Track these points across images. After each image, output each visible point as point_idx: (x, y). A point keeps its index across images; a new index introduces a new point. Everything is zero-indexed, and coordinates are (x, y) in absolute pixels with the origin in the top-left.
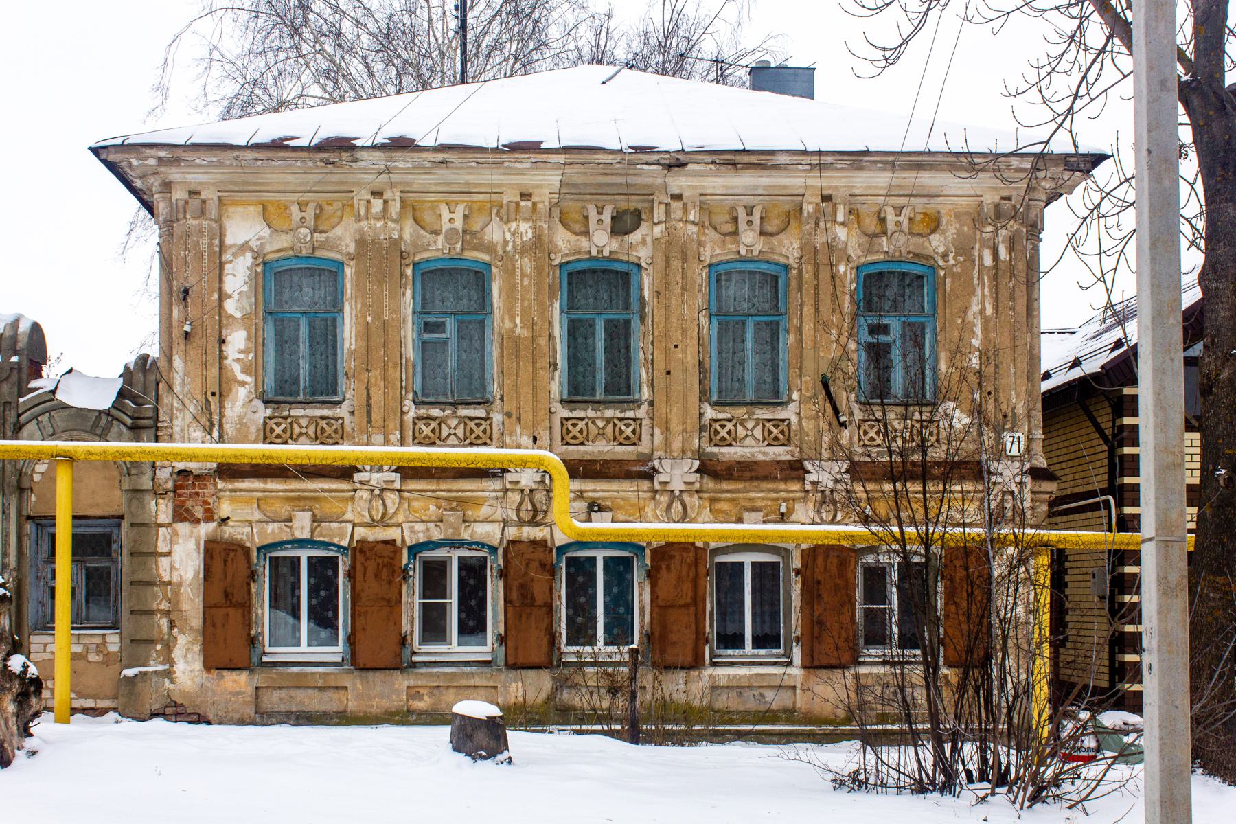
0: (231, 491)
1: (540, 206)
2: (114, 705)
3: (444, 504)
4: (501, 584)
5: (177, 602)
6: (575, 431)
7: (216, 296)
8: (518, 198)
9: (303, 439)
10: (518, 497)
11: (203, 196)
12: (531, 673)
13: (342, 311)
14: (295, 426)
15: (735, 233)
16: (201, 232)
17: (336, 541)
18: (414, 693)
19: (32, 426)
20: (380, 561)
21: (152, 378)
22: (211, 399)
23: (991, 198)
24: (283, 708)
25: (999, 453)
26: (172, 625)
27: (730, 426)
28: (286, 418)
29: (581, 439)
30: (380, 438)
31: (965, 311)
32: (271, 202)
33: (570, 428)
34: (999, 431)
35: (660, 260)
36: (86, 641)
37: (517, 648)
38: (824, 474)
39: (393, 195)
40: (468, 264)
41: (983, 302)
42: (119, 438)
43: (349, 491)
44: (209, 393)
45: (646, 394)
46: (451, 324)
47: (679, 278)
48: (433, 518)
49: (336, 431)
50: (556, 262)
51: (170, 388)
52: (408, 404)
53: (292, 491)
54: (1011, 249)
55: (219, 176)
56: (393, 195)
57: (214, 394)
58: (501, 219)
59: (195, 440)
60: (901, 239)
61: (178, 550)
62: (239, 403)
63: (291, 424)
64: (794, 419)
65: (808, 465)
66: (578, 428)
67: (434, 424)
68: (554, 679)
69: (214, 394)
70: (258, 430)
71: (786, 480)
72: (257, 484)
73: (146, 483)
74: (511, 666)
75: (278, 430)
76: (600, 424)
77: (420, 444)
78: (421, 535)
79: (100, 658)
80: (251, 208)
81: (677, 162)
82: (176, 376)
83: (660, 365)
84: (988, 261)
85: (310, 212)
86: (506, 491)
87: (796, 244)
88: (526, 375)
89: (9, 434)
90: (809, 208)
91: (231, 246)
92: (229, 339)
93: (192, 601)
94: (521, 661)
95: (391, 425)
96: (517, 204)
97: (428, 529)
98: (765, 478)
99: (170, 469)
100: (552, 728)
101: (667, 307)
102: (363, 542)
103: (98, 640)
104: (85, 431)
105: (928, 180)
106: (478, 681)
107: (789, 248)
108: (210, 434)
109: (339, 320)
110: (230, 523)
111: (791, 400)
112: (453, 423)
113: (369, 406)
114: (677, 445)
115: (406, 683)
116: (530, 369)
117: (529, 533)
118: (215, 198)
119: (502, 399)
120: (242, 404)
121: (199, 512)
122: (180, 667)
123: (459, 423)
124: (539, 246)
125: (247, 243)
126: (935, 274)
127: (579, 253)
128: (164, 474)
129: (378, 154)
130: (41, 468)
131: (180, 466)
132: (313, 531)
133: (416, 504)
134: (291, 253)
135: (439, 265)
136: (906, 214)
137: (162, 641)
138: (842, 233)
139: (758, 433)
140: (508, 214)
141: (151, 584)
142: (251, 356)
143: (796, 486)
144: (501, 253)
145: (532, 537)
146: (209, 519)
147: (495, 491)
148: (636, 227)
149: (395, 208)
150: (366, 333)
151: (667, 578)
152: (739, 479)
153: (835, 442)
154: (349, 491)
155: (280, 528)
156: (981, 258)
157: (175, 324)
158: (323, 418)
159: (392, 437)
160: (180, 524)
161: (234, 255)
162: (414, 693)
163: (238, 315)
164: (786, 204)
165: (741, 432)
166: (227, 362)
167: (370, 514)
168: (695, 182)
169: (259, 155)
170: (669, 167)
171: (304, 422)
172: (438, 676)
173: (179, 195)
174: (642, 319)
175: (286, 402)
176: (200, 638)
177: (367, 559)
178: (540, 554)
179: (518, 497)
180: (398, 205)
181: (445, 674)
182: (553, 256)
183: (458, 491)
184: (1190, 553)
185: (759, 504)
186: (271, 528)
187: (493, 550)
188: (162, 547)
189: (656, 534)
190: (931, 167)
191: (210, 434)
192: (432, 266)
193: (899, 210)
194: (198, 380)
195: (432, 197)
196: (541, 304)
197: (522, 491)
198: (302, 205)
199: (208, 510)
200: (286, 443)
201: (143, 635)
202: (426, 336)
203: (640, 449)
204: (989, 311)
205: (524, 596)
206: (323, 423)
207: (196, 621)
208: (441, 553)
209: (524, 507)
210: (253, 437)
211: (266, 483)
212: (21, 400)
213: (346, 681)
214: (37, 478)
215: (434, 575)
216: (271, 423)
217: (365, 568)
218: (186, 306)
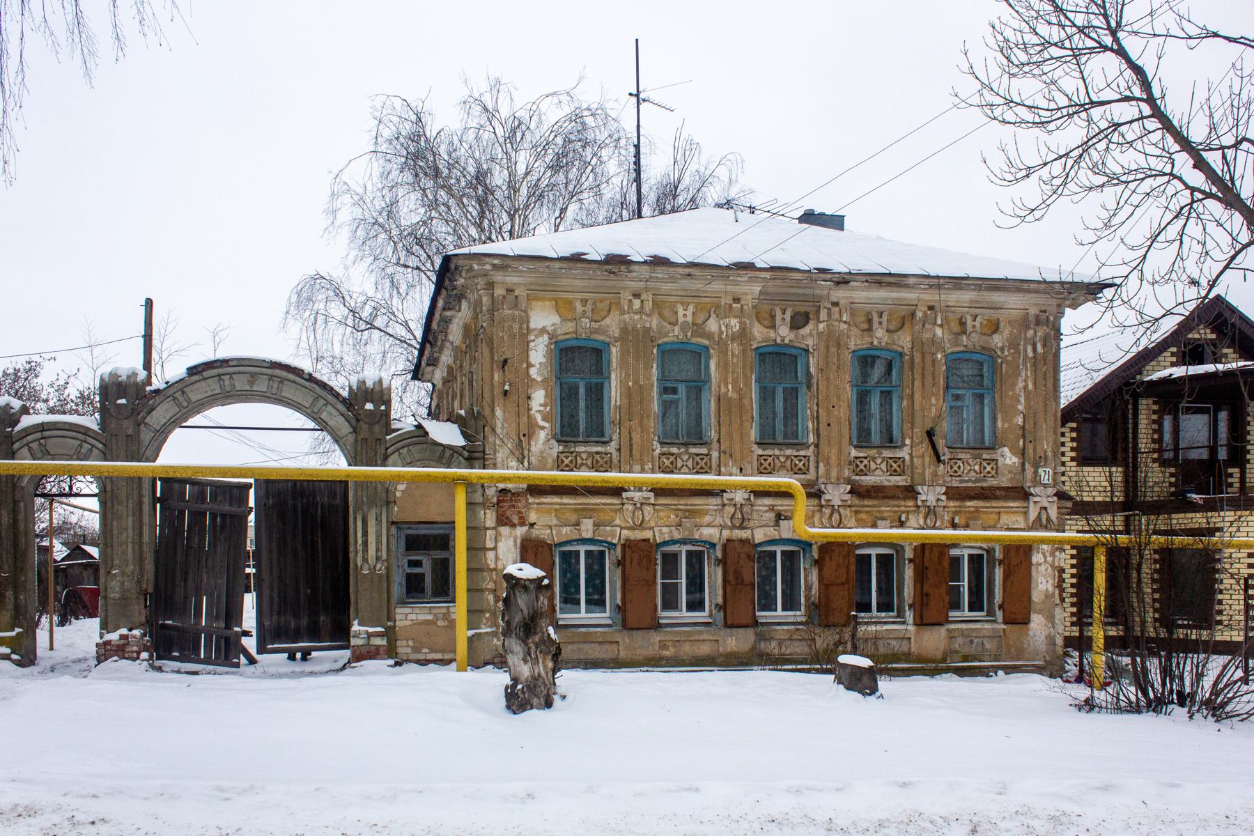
3: (680, 513)
4: (719, 571)
6: (766, 464)
9: (583, 468)
10: (732, 510)
12: (741, 631)
15: (870, 329)
16: (514, 319)
18: (663, 646)
19: (395, 456)
21: (481, 423)
23: (1033, 311)
24: (575, 657)
25: (1036, 481)
27: (866, 462)
30: (638, 467)
31: (1015, 384)
34: (1036, 466)
35: (823, 349)
38: (929, 495)
41: (1026, 381)
45: (811, 439)
46: (682, 389)
47: (835, 360)
51: (494, 430)
52: (656, 445)
54: (1044, 346)
59: (512, 468)
60: (975, 337)
61: (502, 546)
62: (541, 442)
64: (907, 458)
65: (919, 488)
67: (672, 458)
68: (756, 634)
71: (905, 499)
72: (556, 499)
73: (479, 499)
74: (727, 625)
75: (567, 461)
76: (782, 459)
77: (663, 472)
81: (843, 280)
83: (823, 420)
84: (1031, 354)
85: (589, 307)
86: (724, 505)
87: (909, 339)
88: (735, 426)
90: (919, 314)
96: (730, 306)
98: (893, 497)
101: (828, 380)
102: (628, 540)
103: (444, 611)
105: (997, 297)
106: (706, 637)
107: (904, 341)
109: (606, 384)
111: (903, 445)
112: (685, 457)
114: (834, 474)
119: (719, 441)
120: (542, 442)
121: (515, 520)
124: (744, 335)
125: (544, 328)
126: (995, 362)
128: (491, 492)
129: (647, 267)
131: (501, 486)
133: (662, 514)
135: (674, 347)
136: (978, 319)
138: (939, 332)
139: (884, 466)
140: (722, 312)
141: (481, 570)
143: (911, 503)
146: (522, 524)
148: (807, 323)
149: (648, 306)
150: (628, 394)
151: (830, 566)
152: (876, 498)
153: (935, 475)
156: (1025, 351)
157: (496, 384)
158: (598, 453)
161: (536, 336)
162: (663, 646)
163: (539, 379)
164: (904, 310)
165: (873, 466)
168: (848, 294)
169: (564, 265)
170: (838, 283)
171: (584, 456)
172: (679, 633)
173: (499, 292)
174: (809, 387)
178: (747, 549)
179: (732, 510)
185: (886, 515)
186: (565, 530)
187: (713, 545)
188: (489, 544)
189: (819, 535)
190: (1005, 289)
192: (668, 347)
193: (975, 317)
194: (514, 425)
196: (745, 375)
199: (521, 518)
201: (477, 607)
202: (665, 397)
203: (808, 477)
204: (1030, 387)
205: (737, 578)
206: (598, 457)
208: (675, 548)
210: (549, 466)
214: (398, 494)
215: (670, 561)
216: (562, 456)
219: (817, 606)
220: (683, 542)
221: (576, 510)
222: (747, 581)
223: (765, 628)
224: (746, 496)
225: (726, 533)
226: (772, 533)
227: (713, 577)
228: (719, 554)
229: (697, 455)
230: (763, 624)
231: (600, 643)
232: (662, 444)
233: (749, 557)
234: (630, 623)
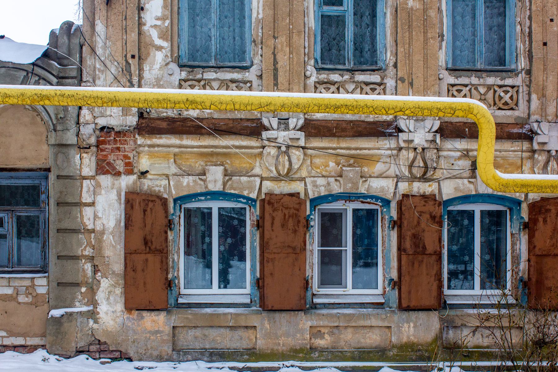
0: (150, 146)
4: (394, 235)
10: (411, 155)
12: (422, 315)
17: (245, 193)
18: (316, 332)
20: (286, 212)
22: (130, 61)
24: (198, 345)
26: (96, 270)
37: (410, 292)
43: (257, 148)
44: (129, 56)
45: (523, 63)
48: (333, 174)
51: (93, 50)
52: (310, 69)
53: (205, 147)
57: (133, 57)
61: (101, 200)
68: (441, 320)
69: (133, 57)
72: (173, 140)
74: (405, 308)
76: (482, 90)
78: (322, 189)
79: (29, 299)
82: (98, 39)
83: (537, 37)
86: (400, 149)
88: (418, 44)
92: (147, 6)
93: (114, 247)
94: (413, 304)
97: (329, 184)
102: (270, 194)
103: (28, 283)
106: (374, 322)
110: (149, 176)
113: (276, 70)
115: (309, 323)
116: (422, 38)
117: (419, 188)
119: (395, 66)
121: (120, 166)
122: (103, 308)
132: (224, 184)
133: (317, 161)
137: (86, 284)
141: (75, 231)
142: (167, 23)
145: (422, 192)
146: (130, 172)
151: (544, 230)
154: (257, 148)
155: (194, 181)
162: (316, 332)
166: (145, 28)
172: (338, 316)
175: (199, 67)
176: (122, 282)
178: (430, 207)
179: (411, 155)
181: (345, 315)
183: (356, 149)
186: (186, 180)
187: (387, 203)
188: (86, 198)
194: (119, 44)
197: (415, 149)
199: (128, 164)
203: (516, 113)
205: (416, 245)
207: (118, 267)
211: (181, 139)
213: (255, 321)
215: (331, 222)
217: (273, 219)
219: (526, 284)
220: (348, 197)
221: (202, 155)
222: (430, 248)
223: (453, 313)
224: (430, 137)
225: (403, 187)
226: (466, 187)
227: (387, 241)
228: (394, 214)
229: (367, 84)
230: (453, 307)
231: (232, 328)
232: (319, 70)
233: (433, 218)
234: (269, 303)
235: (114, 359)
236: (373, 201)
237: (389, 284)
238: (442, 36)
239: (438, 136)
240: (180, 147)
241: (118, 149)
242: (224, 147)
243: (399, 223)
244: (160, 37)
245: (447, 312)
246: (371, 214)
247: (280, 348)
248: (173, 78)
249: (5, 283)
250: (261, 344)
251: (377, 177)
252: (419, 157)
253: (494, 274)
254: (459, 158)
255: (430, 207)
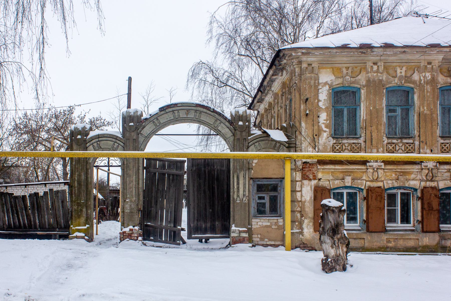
0: (323, 169)
1: (434, 67)
2: (281, 244)
3: (398, 174)
4: (365, 203)
5: (304, 208)
6: (445, 148)
7: (317, 101)
8: (426, 64)
9: (346, 151)
11: (313, 66)
12: (431, 234)
13: (360, 105)
14: (343, 146)
16: (311, 78)
17: (360, 187)
19: (91, 147)
20: (377, 194)
22: (315, 137)
26: (302, 216)
28: (340, 143)
29: (447, 150)
32: (336, 67)
33: (443, 146)
36: (272, 221)
37: (427, 225)
39: (381, 64)
40: (405, 88)
42: (283, 151)
44: (314, 135)
48: (394, 179)
49: (358, 148)
50: (439, 87)
51: (300, 133)
52: (385, 139)
53: (344, 169)
55: (319, 59)
56: (381, 64)
57: (316, 135)
58: (419, 72)
59: (310, 151)
61: (304, 189)
63: (342, 145)
66: (446, 146)
67: (393, 145)
68: (439, 236)
69: (316, 135)
70: (331, 148)
72: (332, 167)
74: (423, 231)
75: (337, 148)
77: (389, 152)
78: (390, 185)
79: (276, 227)
80: (328, 70)
82: (303, 129)
85: (350, 70)
86: (422, 169)
89: (245, 150)
91: (321, 83)
92: (320, 116)
93: (309, 207)
94: (428, 230)
95: (379, 146)
97: (393, 183)
99: (301, 162)
100: (439, 254)
103: (276, 221)
104: (271, 148)
106: (412, 237)
108: (315, 149)
109: (358, 109)
110: (321, 180)
112: (401, 145)
113: (372, 139)
115: (386, 237)
116: (430, 125)
117: (429, 184)
118: (317, 66)
119: (419, 136)
120: (325, 138)
121: (311, 176)
122: (305, 231)
123: (403, 145)
124: (433, 81)
125: (327, 82)
127: (447, 84)
128: (299, 163)
129: (381, 49)
130: (255, 161)
131: (304, 160)
132: (352, 183)
133: (388, 174)
134: (342, 85)
136: (350, 70)
137: (298, 221)
142: (328, 122)
144: (418, 84)
145: (430, 185)
146: (315, 179)
147: (417, 169)
150: (370, 113)
155: (340, 182)
158: (354, 143)
159: (379, 150)
160: (305, 181)
161: (323, 86)
162: (388, 241)
163: (324, 107)
166: (320, 124)
167: (372, 177)
169: (338, 51)
171: (346, 145)
172: (397, 235)
173: (304, 65)
175: (339, 138)
176: (312, 221)
177: (372, 193)
179: (427, 171)
180: (383, 67)
181: (400, 234)
182: (438, 85)
183: (404, 169)
184: (13, 194)
186: (336, 182)
187: (416, 190)
191: (315, 149)
192: (391, 89)
194: (311, 131)
195: (394, 64)
197: (428, 169)
198: (347, 68)
199: (314, 176)
200: (340, 152)
202: (390, 114)
205: (429, 207)
206: (354, 145)
207: (311, 215)
209: (428, 175)
210: (329, 150)
211: (335, 166)
212: (249, 138)
213: (364, 236)
214: (254, 165)
215: (392, 197)
216: (335, 145)
217: (372, 197)
218: (306, 104)
220: (399, 188)
223: (445, 233)
224: (435, 164)
225: (423, 184)
228: (419, 194)
229: (407, 143)
232: (388, 138)
234: (371, 229)
235: (310, 250)
236: (410, 189)
237: (417, 222)
238: (438, 124)
239: (438, 164)
240: (334, 169)
241: (310, 170)
242: (351, 169)
243: (367, 198)
244: (325, 127)
245: (442, 233)
246: (408, 195)
247: (375, 247)
248: (330, 143)
249: (267, 221)
250: (367, 245)
251: (412, 180)
252: (430, 172)
253: (405, 219)
254: (446, 172)
255: (435, 192)
